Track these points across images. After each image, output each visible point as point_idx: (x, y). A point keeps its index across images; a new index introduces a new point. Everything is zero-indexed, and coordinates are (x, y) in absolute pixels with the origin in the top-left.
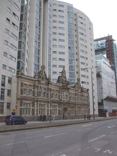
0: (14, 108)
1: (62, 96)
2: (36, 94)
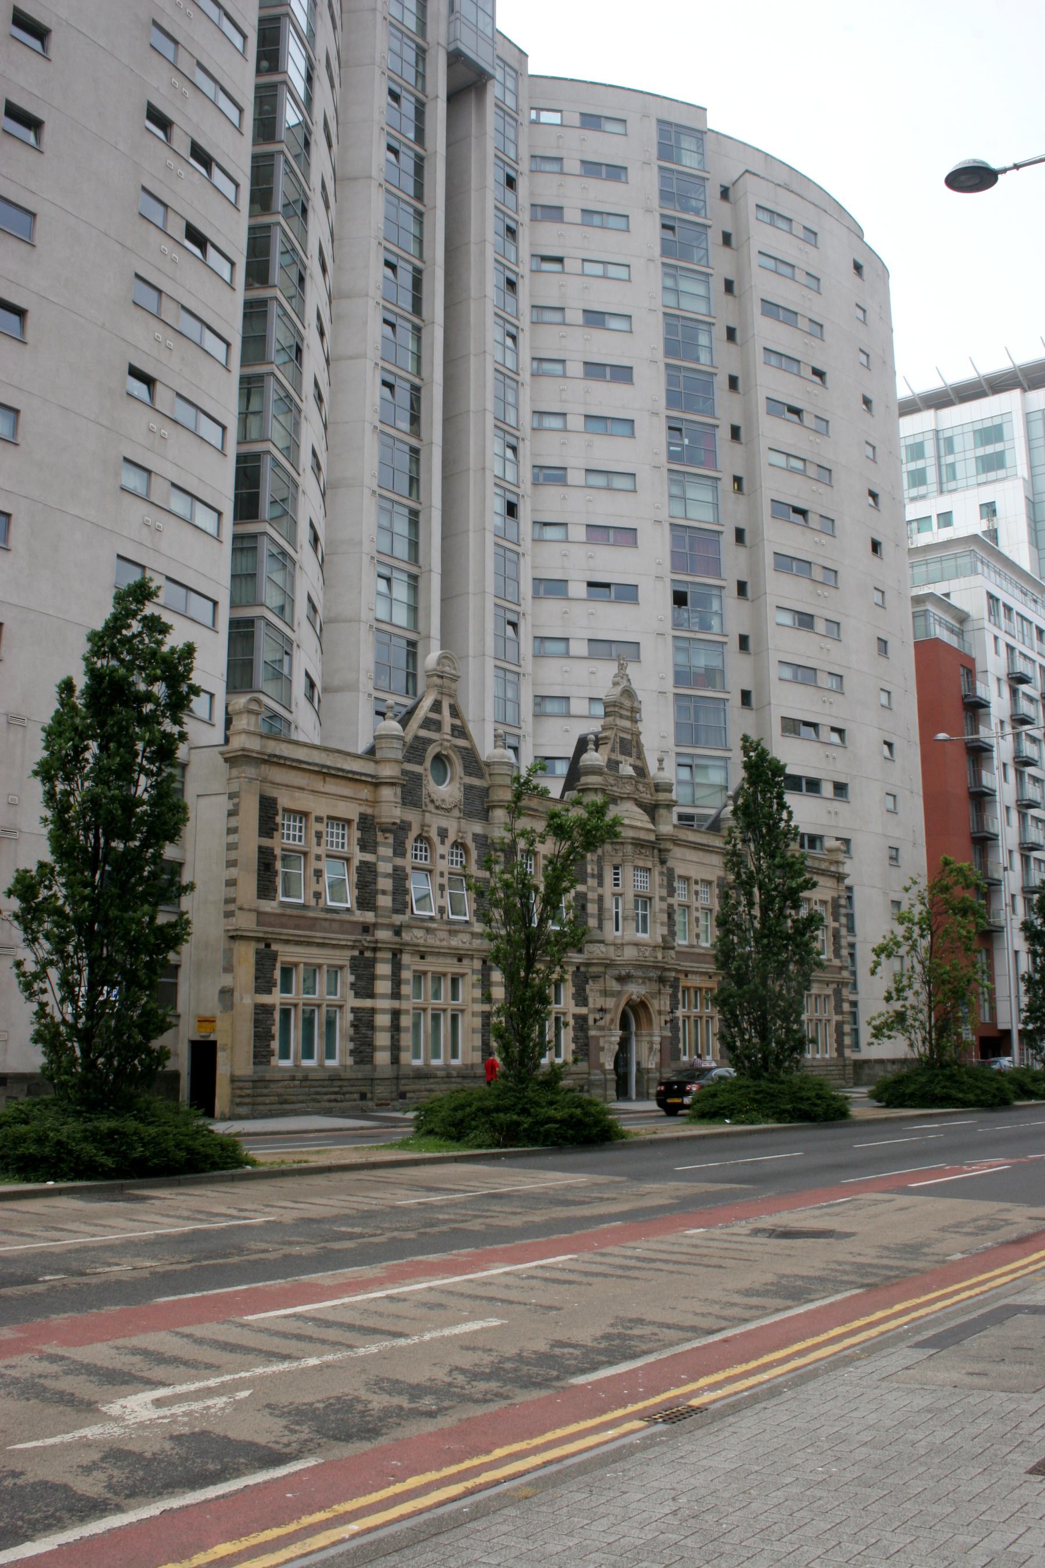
0: (211, 1005)
1: (609, 903)
2: (384, 892)
